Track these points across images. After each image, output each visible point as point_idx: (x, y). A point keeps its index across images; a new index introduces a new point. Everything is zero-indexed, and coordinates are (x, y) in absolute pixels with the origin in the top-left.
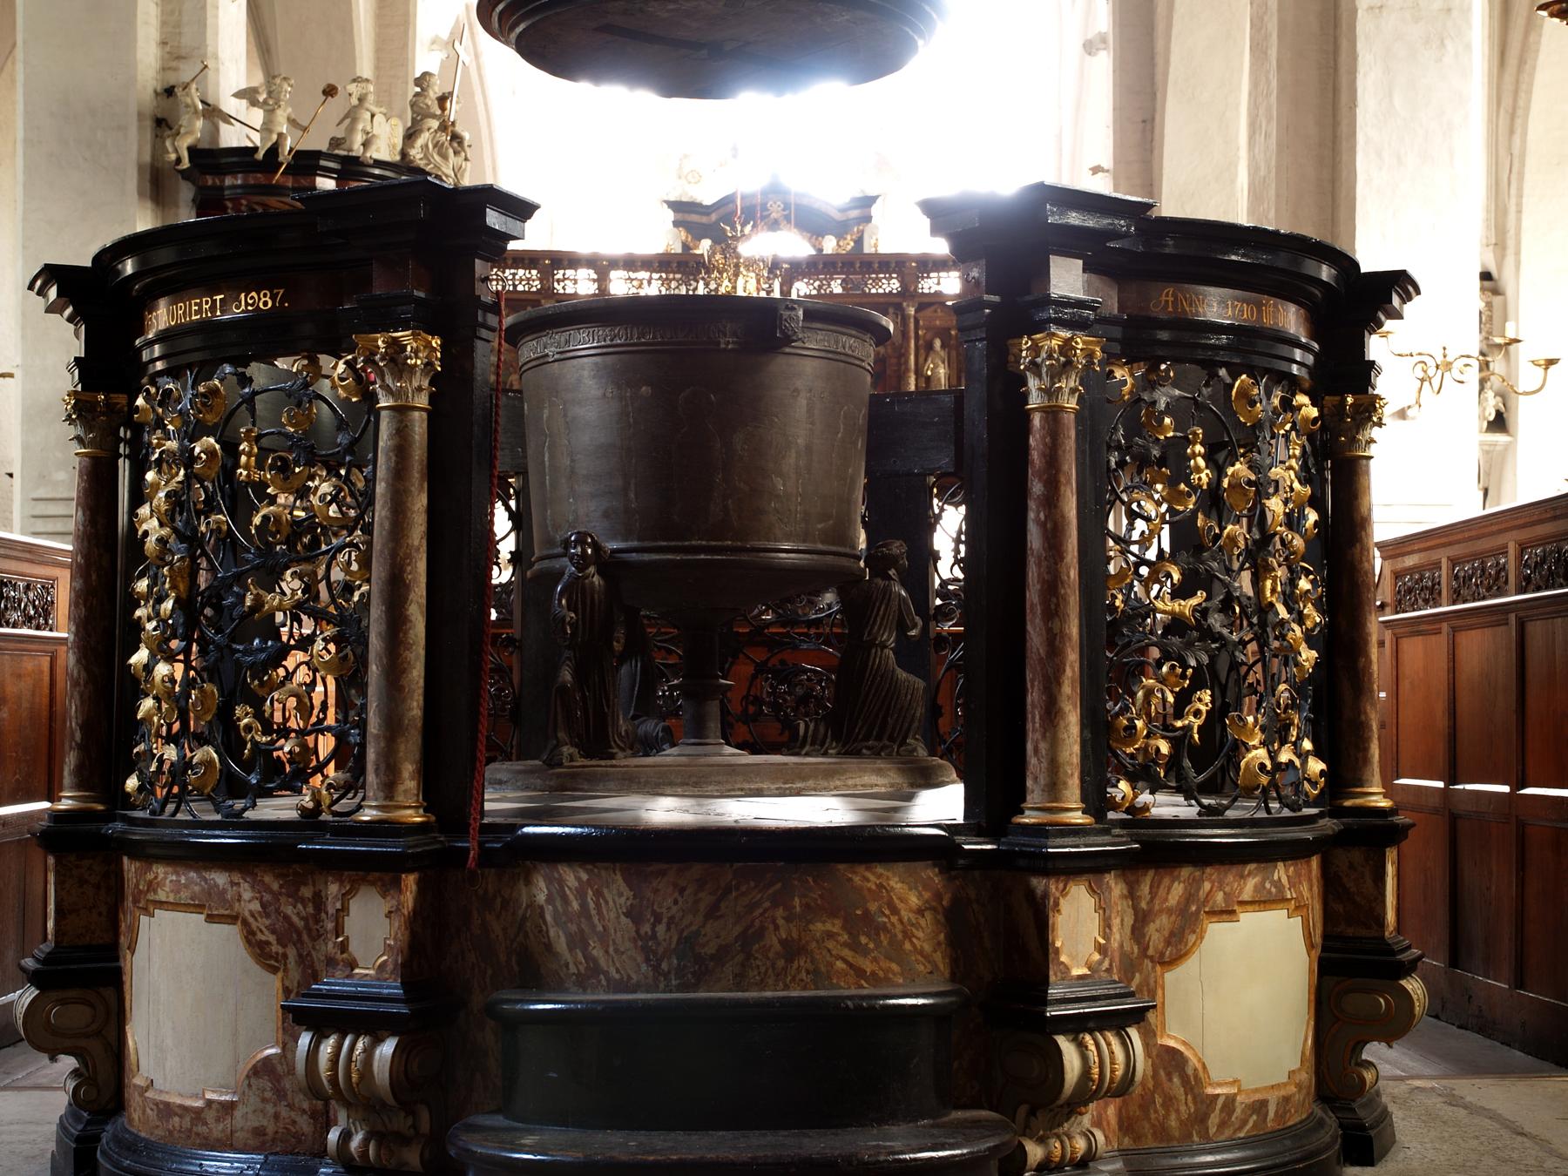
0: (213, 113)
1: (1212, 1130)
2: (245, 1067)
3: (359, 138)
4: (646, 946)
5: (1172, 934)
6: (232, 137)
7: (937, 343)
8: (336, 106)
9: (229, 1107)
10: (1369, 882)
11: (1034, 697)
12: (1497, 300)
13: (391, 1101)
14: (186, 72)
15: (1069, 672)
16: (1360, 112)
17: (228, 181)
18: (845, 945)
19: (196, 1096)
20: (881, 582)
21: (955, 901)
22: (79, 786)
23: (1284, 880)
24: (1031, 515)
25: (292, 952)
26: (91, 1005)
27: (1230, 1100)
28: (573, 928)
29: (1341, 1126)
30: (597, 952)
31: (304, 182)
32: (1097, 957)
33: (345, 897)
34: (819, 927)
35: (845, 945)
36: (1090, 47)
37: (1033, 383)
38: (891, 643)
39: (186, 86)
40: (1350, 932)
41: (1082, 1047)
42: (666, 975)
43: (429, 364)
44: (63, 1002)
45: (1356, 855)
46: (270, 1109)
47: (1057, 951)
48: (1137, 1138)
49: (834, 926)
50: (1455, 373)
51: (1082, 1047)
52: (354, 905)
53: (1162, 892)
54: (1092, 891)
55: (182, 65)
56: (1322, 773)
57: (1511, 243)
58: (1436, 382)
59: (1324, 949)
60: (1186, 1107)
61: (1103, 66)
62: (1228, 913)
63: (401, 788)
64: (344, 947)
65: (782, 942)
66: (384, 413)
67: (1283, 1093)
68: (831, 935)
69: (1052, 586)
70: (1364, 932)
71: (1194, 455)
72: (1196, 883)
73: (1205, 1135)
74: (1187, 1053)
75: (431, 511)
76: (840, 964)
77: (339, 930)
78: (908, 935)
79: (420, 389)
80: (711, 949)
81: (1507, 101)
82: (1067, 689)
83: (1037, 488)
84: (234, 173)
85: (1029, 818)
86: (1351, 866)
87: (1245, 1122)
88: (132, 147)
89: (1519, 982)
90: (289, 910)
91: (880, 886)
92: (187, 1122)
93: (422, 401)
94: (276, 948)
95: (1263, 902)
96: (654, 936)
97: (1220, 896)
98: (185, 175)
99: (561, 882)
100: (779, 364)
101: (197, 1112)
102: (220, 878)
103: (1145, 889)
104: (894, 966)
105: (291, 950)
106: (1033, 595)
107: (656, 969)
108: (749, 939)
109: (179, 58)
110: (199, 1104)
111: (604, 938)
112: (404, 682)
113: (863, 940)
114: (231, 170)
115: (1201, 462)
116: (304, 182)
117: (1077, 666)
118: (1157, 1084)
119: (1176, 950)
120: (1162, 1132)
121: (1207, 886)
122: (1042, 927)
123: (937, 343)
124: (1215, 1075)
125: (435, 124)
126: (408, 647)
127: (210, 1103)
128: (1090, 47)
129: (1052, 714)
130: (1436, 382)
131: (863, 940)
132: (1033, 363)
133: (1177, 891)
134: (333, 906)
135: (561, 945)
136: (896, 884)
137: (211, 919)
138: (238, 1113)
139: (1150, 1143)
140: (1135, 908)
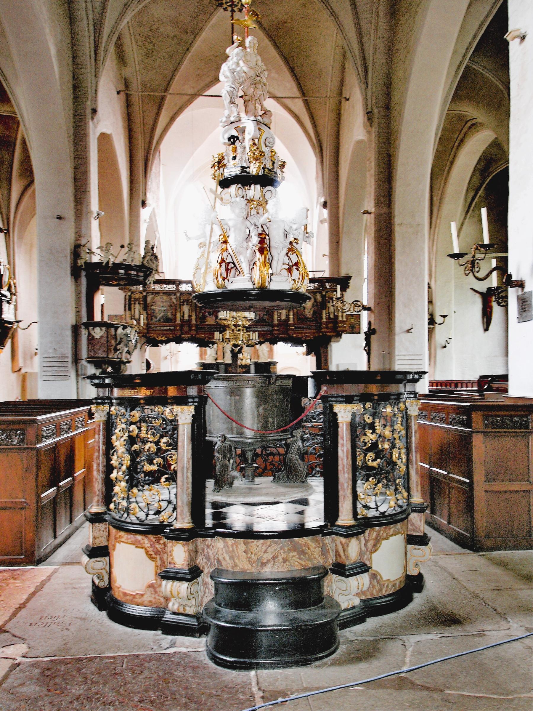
0: (91, 253)
2: (146, 585)
3: (131, 259)
6: (95, 259)
9: (142, 595)
19: (133, 591)
25: (158, 557)
28: (230, 554)
30: (237, 561)
36: (322, 222)
39: (84, 246)
46: (153, 596)
61: (326, 227)
62: (387, 538)
65: (283, 558)
68: (294, 556)
80: (265, 561)
81: (432, 237)
89: (449, 523)
97: (385, 535)
98: (84, 269)
99: (227, 543)
102: (139, 537)
110: (134, 594)
111: (238, 557)
125: (150, 254)
128: (322, 222)
138: (145, 596)
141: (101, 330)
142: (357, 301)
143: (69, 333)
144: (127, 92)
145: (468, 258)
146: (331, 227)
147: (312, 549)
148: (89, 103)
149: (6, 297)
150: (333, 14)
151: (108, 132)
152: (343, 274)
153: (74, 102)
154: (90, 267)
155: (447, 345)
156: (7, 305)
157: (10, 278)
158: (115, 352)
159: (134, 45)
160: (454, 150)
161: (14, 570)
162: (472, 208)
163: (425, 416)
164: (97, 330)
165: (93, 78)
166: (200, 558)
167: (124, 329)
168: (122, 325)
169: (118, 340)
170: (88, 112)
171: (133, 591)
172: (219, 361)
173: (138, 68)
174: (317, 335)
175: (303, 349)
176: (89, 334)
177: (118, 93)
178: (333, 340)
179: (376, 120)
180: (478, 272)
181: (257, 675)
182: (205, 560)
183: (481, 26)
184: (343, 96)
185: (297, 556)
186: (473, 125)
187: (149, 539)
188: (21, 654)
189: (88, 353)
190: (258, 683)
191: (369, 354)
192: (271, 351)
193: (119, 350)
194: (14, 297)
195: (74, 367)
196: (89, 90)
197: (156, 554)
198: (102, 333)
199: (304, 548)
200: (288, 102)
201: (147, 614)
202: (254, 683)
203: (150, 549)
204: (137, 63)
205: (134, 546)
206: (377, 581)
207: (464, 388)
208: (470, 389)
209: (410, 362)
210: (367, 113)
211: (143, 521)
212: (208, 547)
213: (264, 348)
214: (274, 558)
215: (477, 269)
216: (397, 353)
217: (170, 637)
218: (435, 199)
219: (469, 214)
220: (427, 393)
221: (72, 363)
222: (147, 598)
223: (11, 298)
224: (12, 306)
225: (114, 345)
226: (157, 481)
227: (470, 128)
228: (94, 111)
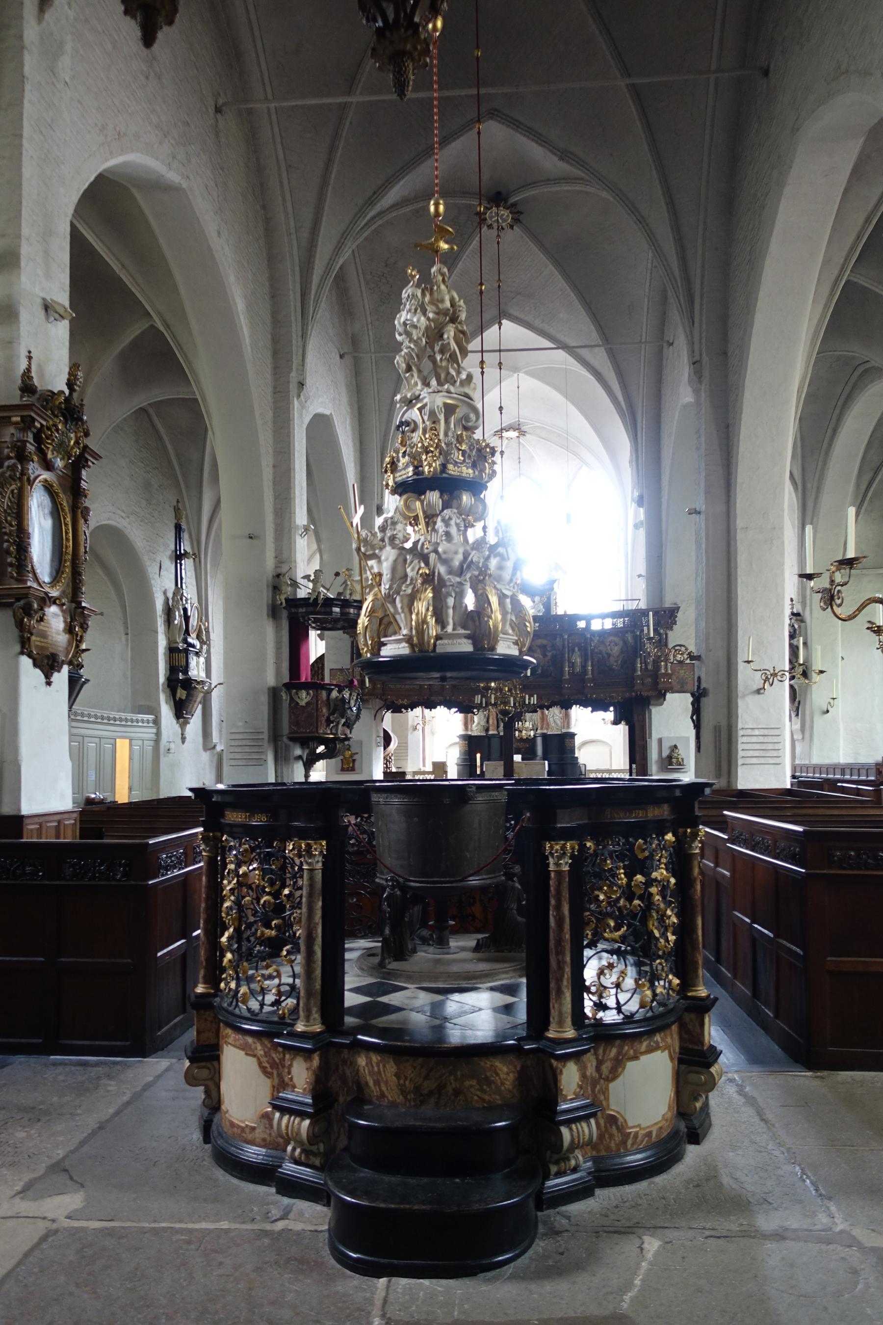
1: (629, 1146)
3: (348, 592)
4: (403, 1091)
5: (612, 1068)
6: (302, 593)
7: (576, 649)
8: (340, 579)
9: (253, 1129)
10: (698, 1027)
11: (552, 985)
12: (803, 624)
13: (306, 1142)
14: (284, 569)
15: (566, 976)
16: (739, 570)
17: (300, 610)
18: (478, 1090)
19: (243, 1122)
20: (510, 882)
21: (522, 1068)
22: (205, 983)
23: (659, 1039)
24: (551, 913)
25: (275, 1072)
26: (208, 1068)
27: (636, 1135)
28: (375, 1078)
29: (687, 1127)
30: (384, 1089)
31: (328, 610)
32: (578, 1090)
33: (292, 1060)
34: (467, 1083)
35: (478, 1090)
36: (636, 526)
37: (551, 861)
38: (515, 907)
39: (284, 575)
40: (690, 1046)
41: (571, 1130)
42: (409, 1101)
43: (321, 852)
44: (199, 1068)
45: (693, 1016)
46: (268, 1131)
47: (561, 1090)
48: (598, 1151)
49: (474, 1082)
50: (779, 678)
51: (571, 1130)
52: (295, 1064)
53: (607, 1052)
54: (576, 1064)
55: (283, 565)
56: (678, 985)
57: (808, 601)
58: (771, 681)
59: (680, 1053)
60: (618, 1138)
62: (636, 1058)
63: (312, 1018)
64: (291, 1079)
66: (305, 871)
67: (659, 1125)
68: (472, 1086)
69: (559, 942)
70: (696, 1047)
71: (620, 874)
72: (621, 1048)
73: (626, 1148)
74: (618, 1116)
75: (323, 907)
76: (475, 1098)
77: (289, 1073)
78: (503, 1084)
79: (318, 862)
80: (426, 1092)
82: (565, 983)
83: (553, 902)
84: (302, 607)
85: (551, 1034)
86: (691, 1020)
87: (642, 1141)
88: (265, 597)
90: (274, 1055)
91: (492, 1066)
92: (239, 1132)
93: (320, 865)
94: (269, 1070)
95: (650, 1050)
96: (405, 1085)
97: (632, 1052)
99: (371, 1059)
100: (467, 808)
101: (243, 1129)
102: (250, 1040)
103: (601, 1051)
104: (498, 1097)
105: (275, 1072)
106: (552, 944)
107: (406, 1098)
108: (441, 1088)
109: (282, 563)
110: (243, 1125)
111: (386, 1083)
112: (313, 976)
113: (485, 1087)
114: (301, 606)
115: (623, 876)
116: (328, 610)
117: (569, 974)
118: (606, 1130)
119: (614, 1074)
120: (608, 1148)
121: (626, 1048)
122: (556, 1081)
123: (576, 649)
124: (630, 1124)
126: (314, 962)
127: (247, 1126)
129: (559, 992)
130: (771, 681)
131: (485, 1087)
132: (550, 852)
133: (614, 1051)
134: (287, 1063)
135: (371, 1083)
136: (498, 1064)
137: (247, 1054)
138: (257, 1131)
139: (603, 1153)
140: (597, 1059)
141: (308, 694)
142: (680, 646)
143: (264, 699)
144: (356, 354)
145: (823, 583)
146: (648, 536)
147: (502, 1076)
148: (293, 374)
149: (193, 646)
150: (642, 221)
151: (327, 412)
152: (667, 604)
153: (275, 374)
154: (293, 603)
155: (829, 708)
156: (195, 658)
157: (200, 619)
158: (328, 725)
159: (363, 288)
160: (837, 411)
161: (115, 1063)
162: (868, 498)
163: (745, 840)
164: (303, 694)
165: (300, 339)
166: (333, 1078)
167: (340, 692)
168: (336, 686)
169: (332, 708)
170: (293, 387)
171: (243, 1122)
172: (491, 732)
173: (369, 320)
174: (627, 695)
175: (610, 715)
176: (292, 699)
177: (341, 357)
178: (652, 702)
179: (706, 373)
180: (839, 606)
181: (388, 1287)
182: (339, 1083)
183: (867, 221)
184: (666, 338)
185: (478, 1087)
186: (866, 371)
187: (262, 1044)
188: (66, 1214)
189: (290, 727)
190: (385, 1301)
191: (697, 726)
192: (567, 717)
193: (332, 722)
194: (205, 647)
195: (272, 746)
196: (294, 357)
197: (272, 1067)
198: (309, 698)
199: (488, 1074)
200: (583, 352)
201: (259, 1159)
202: (378, 1302)
203: (264, 1059)
204: (368, 313)
205: (242, 1053)
206: (618, 1128)
207: (855, 778)
208: (864, 778)
209: (761, 739)
210: (694, 363)
211: (257, 1015)
212: (344, 1062)
213: (555, 713)
214: (441, 1088)
215: (839, 602)
216: (740, 726)
217: (286, 1201)
218: (809, 486)
219: (864, 508)
220: (789, 787)
221: (269, 741)
222: (259, 1134)
223: (201, 647)
224: (202, 660)
225: (326, 715)
226: (275, 954)
227: (861, 376)
228: (301, 385)
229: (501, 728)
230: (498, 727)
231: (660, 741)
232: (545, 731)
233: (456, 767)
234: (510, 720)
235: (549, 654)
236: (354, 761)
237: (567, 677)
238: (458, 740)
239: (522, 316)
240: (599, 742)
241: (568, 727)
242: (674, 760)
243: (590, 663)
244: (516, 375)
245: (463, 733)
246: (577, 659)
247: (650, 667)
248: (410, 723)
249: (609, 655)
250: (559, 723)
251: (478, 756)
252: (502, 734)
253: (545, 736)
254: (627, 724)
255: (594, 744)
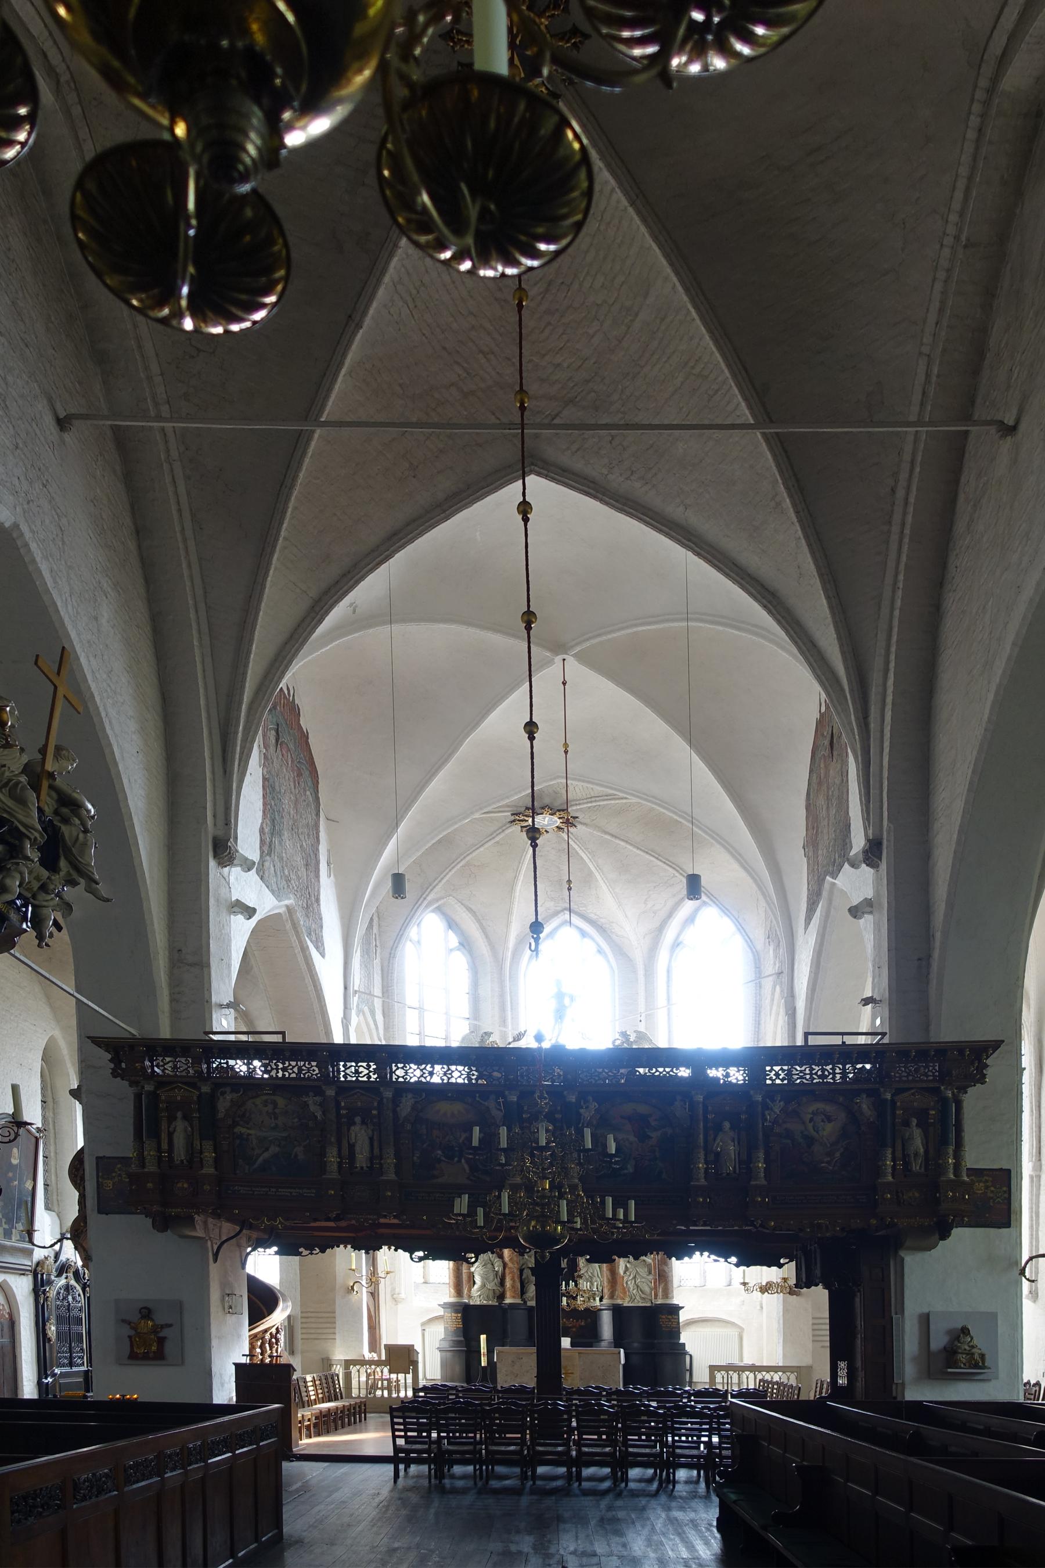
123: (727, 1125)
177: (63, 423)
229: (532, 1290)
230: (523, 1292)
231: (925, 1320)
232: (619, 1302)
233: (438, 1354)
234: (550, 1276)
235: (655, 1135)
236: (161, 1341)
237: (703, 1182)
238: (441, 1312)
239: (578, 465)
240: (737, 1318)
241: (667, 1292)
242: (962, 1358)
243: (761, 1155)
244: (558, 659)
245: (452, 1300)
246: (729, 1147)
247: (916, 1167)
248: (339, 1280)
249: (810, 1141)
250: (647, 1289)
251: (483, 1337)
252: (532, 1303)
253: (618, 1311)
254: (825, 1288)
255: (709, 1324)
